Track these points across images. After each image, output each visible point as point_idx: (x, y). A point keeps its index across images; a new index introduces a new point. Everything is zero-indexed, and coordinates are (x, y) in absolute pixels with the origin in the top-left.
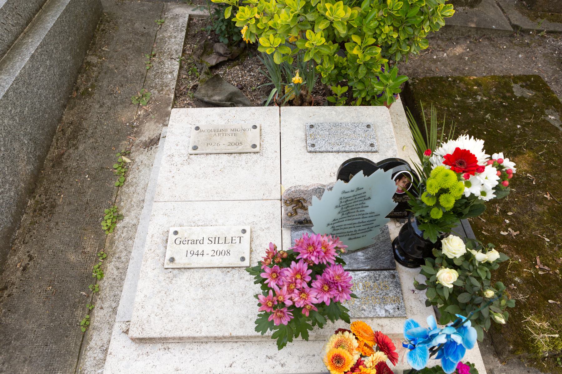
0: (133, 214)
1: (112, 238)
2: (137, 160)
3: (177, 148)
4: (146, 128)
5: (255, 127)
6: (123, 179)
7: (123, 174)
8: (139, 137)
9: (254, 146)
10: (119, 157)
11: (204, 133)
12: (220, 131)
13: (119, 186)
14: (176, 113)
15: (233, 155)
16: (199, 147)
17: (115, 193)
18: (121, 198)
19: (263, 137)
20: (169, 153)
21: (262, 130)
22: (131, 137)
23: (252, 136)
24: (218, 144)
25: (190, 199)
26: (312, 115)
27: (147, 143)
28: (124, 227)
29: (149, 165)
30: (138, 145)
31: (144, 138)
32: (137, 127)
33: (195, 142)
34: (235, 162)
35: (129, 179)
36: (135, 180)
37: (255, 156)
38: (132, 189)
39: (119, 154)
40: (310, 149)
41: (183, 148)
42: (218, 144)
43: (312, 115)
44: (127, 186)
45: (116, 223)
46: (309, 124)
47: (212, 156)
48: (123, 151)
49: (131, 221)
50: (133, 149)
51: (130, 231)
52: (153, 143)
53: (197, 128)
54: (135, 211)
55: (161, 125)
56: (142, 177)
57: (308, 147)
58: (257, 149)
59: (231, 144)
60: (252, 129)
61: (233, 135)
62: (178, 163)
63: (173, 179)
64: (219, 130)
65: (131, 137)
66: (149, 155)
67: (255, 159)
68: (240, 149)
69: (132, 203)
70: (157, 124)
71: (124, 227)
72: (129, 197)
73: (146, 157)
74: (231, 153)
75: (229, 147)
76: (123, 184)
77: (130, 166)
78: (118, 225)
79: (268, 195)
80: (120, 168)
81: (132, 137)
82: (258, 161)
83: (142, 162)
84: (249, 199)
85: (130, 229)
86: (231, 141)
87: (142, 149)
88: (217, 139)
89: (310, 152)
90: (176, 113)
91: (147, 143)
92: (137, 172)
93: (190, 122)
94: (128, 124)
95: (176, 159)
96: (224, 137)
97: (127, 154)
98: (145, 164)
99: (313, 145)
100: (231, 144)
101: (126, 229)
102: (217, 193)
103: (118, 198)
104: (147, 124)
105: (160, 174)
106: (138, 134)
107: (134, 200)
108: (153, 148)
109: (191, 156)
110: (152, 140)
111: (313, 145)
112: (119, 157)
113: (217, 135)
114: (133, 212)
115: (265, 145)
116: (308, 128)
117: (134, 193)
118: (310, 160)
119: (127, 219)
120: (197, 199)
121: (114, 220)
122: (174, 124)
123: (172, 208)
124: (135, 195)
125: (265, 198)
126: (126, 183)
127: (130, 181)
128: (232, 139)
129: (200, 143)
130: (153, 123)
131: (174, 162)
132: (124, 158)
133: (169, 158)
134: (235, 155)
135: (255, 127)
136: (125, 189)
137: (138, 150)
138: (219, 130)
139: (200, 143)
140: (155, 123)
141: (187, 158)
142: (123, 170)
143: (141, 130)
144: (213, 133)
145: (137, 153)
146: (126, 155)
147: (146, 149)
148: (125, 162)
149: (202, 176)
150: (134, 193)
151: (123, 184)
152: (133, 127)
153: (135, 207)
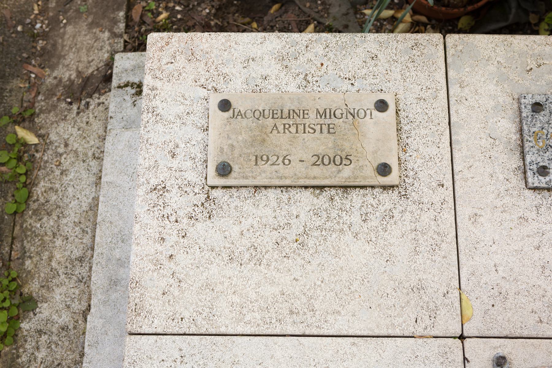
0: (58, 297)
1: (13, 360)
2: (53, 137)
3: (175, 164)
4: (68, 43)
5: (382, 106)
6: (24, 192)
7: (23, 179)
8: (53, 68)
9: (384, 169)
10: (6, 126)
11: (245, 122)
12: (287, 117)
13: (15, 213)
14: (161, 49)
15: (328, 193)
16: (236, 168)
17: (7, 233)
18: (23, 248)
19: (404, 136)
20: (154, 182)
21: (402, 114)
22: (31, 68)
23: (375, 137)
24: (286, 160)
25: (223, 330)
26: (533, 65)
27: (75, 87)
28: (40, 332)
29: (86, 155)
30: (51, 93)
31: (66, 72)
32: (44, 35)
33: (222, 150)
34: (334, 214)
35: (39, 190)
36: (53, 198)
37: (387, 199)
38: (49, 223)
39: (6, 119)
40: (534, 180)
41: (189, 163)
42: (286, 160)
43: (533, 65)
44: (36, 212)
45: (18, 318)
46: (529, 101)
47: (271, 193)
48: (15, 110)
49: (55, 317)
50: (41, 102)
51: (57, 345)
52: (89, 89)
53: (225, 105)
54: (63, 289)
55: (107, 34)
56: (70, 189)
57: (529, 174)
58: (392, 179)
59: (320, 160)
60: (376, 113)
61: (325, 128)
62: (181, 213)
63: (172, 265)
64: (286, 112)
65: (31, 68)
66: (83, 125)
67: (388, 206)
68: (346, 174)
69: (54, 264)
70: (96, 30)
71: (40, 332)
72: (43, 245)
73: (75, 131)
74: (322, 188)
75: (316, 171)
76: (23, 207)
77: (38, 155)
78: (25, 325)
79: (428, 322)
80: (14, 162)
81: (34, 70)
82: (396, 213)
83: (66, 145)
84: (377, 332)
85: (55, 338)
86: (321, 150)
87: (63, 105)
88: (280, 141)
89: (535, 189)
90: (161, 49)
91: (75, 87)
92: (58, 172)
93: (203, 81)
94: (19, 28)
95: (175, 199)
96: (301, 135)
97: (26, 118)
98: (76, 152)
99: (543, 171)
100: (320, 160)
101: (44, 338)
102: (292, 312)
103: (17, 245)
104: (70, 29)
105: (134, 247)
106: (50, 57)
107: (58, 255)
108: (93, 102)
109: (215, 193)
110: (87, 80)
111: (543, 171)
112: (6, 126)
113: (281, 128)
114: (57, 291)
115: (414, 163)
116: (526, 112)
117: (54, 235)
118: (534, 215)
119: (44, 311)
120: (240, 330)
121: (14, 311)
122: (158, 84)
123: (177, 355)
124: (59, 242)
125: (420, 331)
126: (34, 206)
127: (42, 200)
128: (322, 144)
129: (237, 152)
130: (83, 25)
131: (168, 210)
132: (22, 133)
133: (154, 195)
134: (333, 191)
135: (382, 106)
136: (30, 221)
137: (54, 107)
138: (286, 112)
139: (237, 152)
140: (91, 26)
141: (203, 197)
142: (22, 170)
143: (54, 45)
144: (270, 122)
145: (52, 117)
146: (24, 120)
147: (75, 107)
148: (25, 144)
149: (247, 256)
150: (54, 235)
151: (23, 207)
152: (35, 37)
153: (63, 276)
